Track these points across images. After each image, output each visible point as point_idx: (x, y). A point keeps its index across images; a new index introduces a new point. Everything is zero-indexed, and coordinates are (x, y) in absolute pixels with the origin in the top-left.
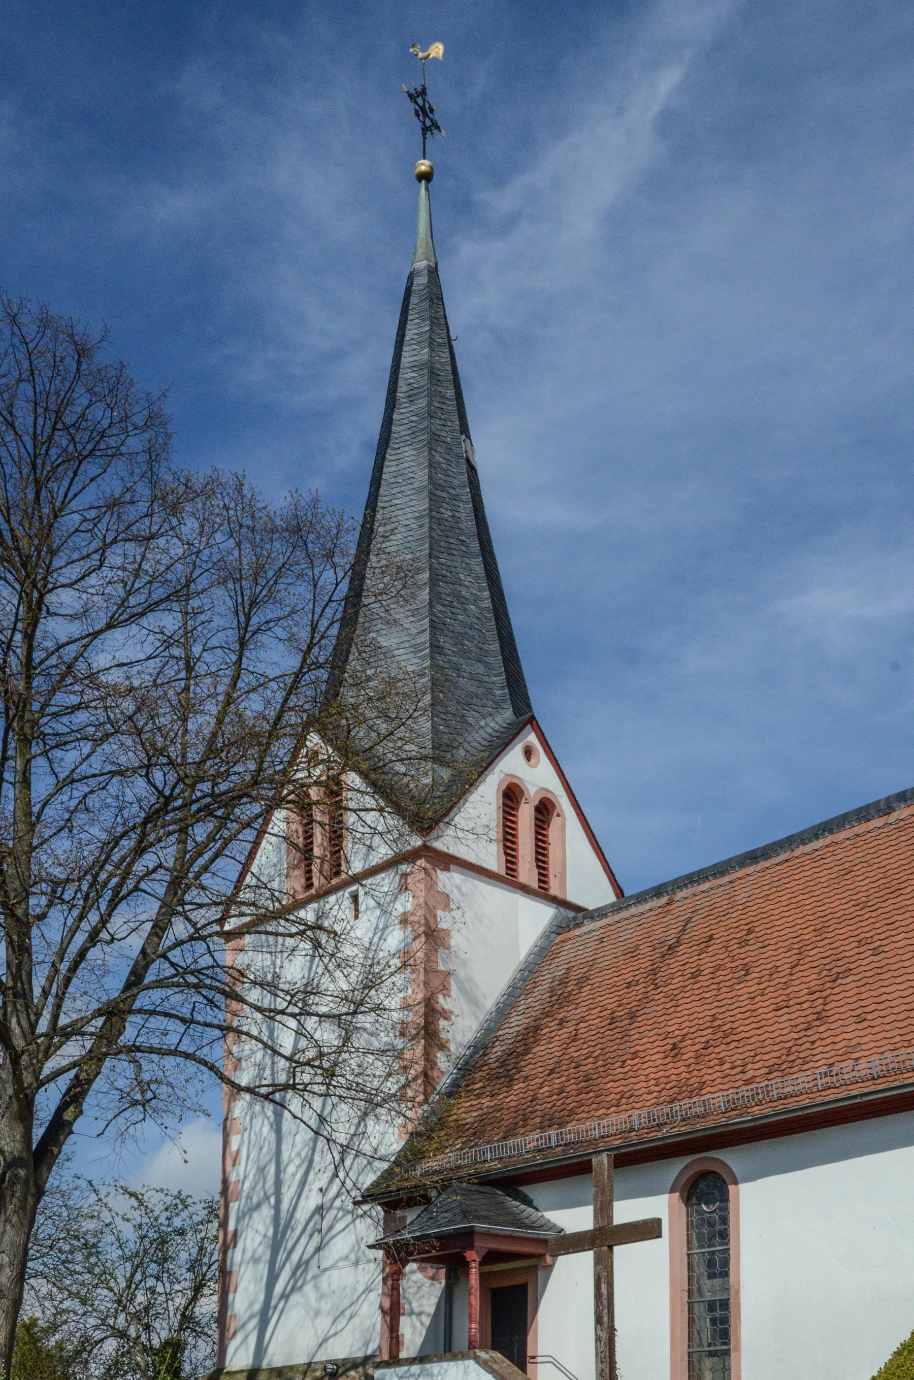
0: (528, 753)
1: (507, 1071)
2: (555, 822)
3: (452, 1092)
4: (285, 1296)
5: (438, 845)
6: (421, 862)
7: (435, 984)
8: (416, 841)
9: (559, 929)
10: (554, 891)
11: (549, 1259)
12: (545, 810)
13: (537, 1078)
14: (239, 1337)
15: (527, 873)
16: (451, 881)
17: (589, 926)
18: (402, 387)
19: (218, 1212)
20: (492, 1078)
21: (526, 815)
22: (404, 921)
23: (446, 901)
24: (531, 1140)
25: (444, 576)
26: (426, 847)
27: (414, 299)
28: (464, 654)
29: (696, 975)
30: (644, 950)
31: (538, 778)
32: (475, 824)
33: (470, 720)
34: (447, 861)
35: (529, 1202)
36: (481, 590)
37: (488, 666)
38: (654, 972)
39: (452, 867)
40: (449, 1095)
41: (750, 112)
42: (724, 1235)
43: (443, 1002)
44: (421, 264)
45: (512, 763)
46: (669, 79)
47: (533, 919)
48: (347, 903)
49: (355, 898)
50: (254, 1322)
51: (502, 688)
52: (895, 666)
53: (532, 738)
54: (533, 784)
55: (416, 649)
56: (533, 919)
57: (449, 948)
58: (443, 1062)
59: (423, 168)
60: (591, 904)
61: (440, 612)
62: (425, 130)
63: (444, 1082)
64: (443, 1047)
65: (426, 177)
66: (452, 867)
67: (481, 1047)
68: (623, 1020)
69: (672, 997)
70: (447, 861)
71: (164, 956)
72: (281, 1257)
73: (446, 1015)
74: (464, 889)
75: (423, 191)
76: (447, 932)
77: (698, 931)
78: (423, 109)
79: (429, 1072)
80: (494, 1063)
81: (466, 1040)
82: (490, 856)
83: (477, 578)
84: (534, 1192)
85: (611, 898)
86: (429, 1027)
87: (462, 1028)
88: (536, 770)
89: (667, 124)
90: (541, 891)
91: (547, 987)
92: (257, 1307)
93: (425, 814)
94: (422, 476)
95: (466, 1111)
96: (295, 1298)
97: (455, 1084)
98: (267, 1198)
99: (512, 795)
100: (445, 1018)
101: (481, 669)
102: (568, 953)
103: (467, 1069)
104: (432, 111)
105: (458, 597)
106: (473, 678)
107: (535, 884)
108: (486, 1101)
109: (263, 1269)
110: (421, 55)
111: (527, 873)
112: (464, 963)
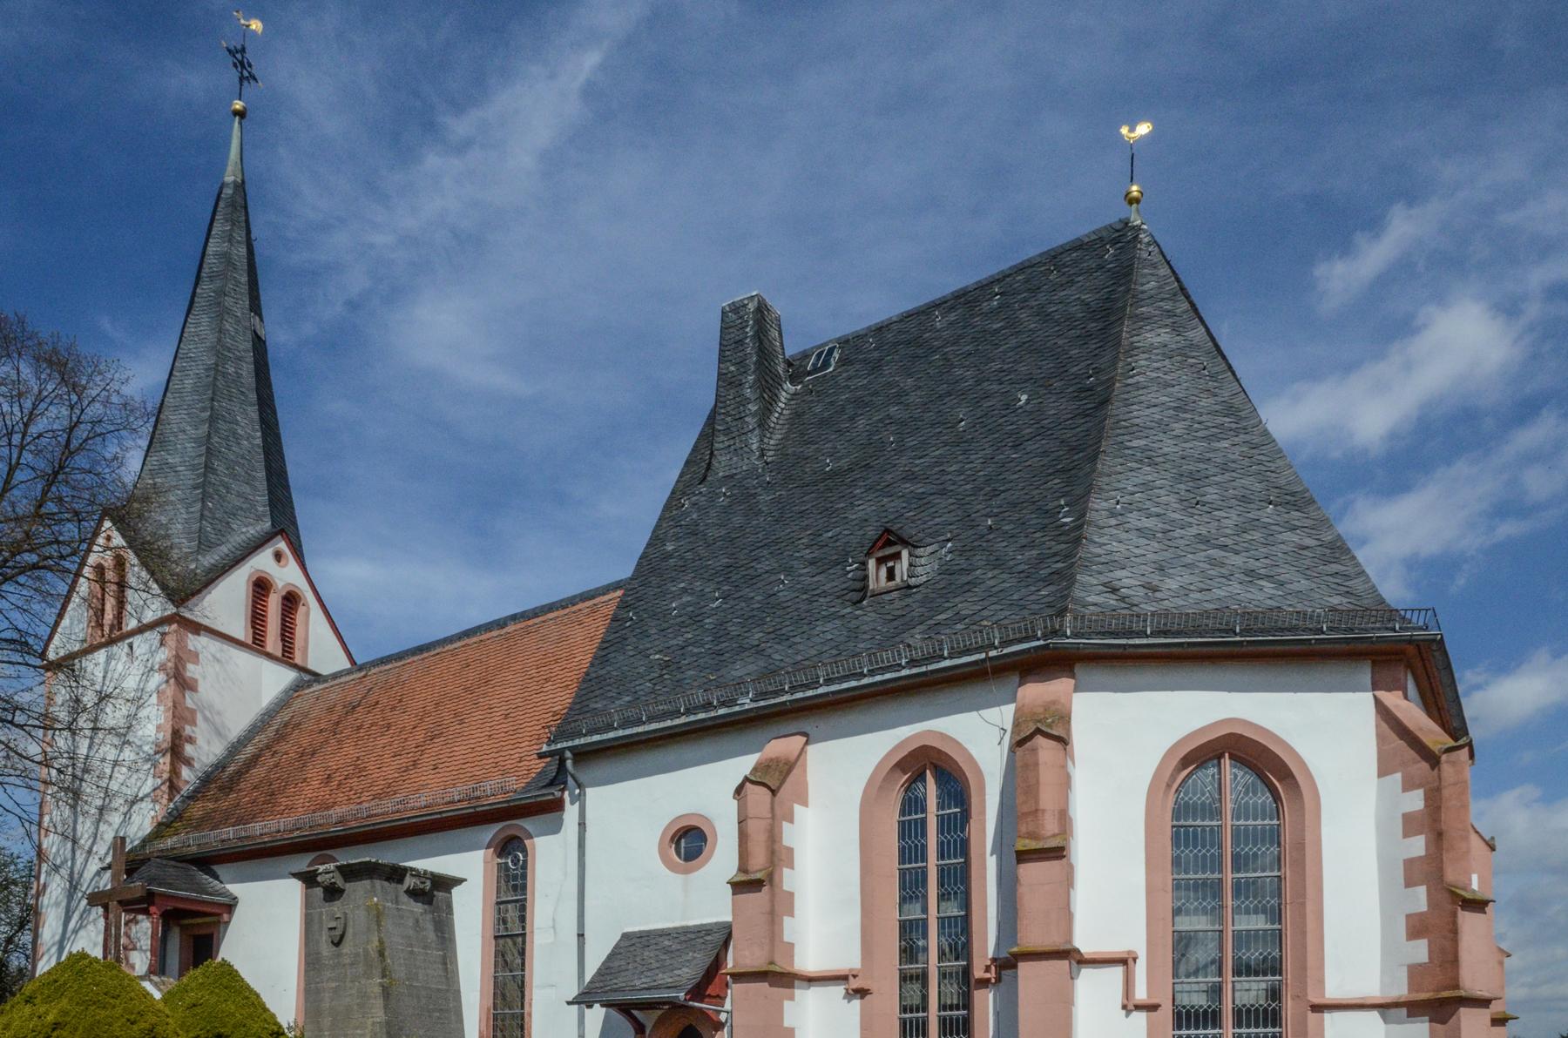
0: (278, 556)
1: (230, 785)
2: (301, 610)
3: (192, 797)
4: (76, 932)
5: (187, 615)
6: (174, 626)
8: (171, 609)
9: (297, 687)
10: (298, 660)
11: (225, 917)
12: (291, 601)
13: (244, 795)
14: (45, 958)
15: (273, 643)
17: (316, 687)
18: (206, 269)
19: (32, 873)
20: (221, 789)
21: (274, 604)
22: (162, 668)
24: (229, 832)
26: (177, 614)
27: (221, 204)
28: (234, 476)
29: (359, 728)
30: (339, 708)
31: (287, 575)
32: (225, 604)
35: (216, 877)
37: (254, 488)
38: (338, 723)
41: (653, 94)
43: (188, 730)
45: (263, 561)
46: (592, 59)
47: (273, 680)
48: (126, 649)
49: (131, 647)
50: (54, 949)
53: (282, 545)
55: (193, 468)
56: (273, 680)
58: (185, 773)
60: (325, 671)
62: (242, 79)
63: (186, 789)
64: (188, 762)
65: (241, 114)
67: (220, 766)
68: (307, 755)
69: (340, 742)
72: (74, 904)
73: (191, 740)
75: (236, 125)
77: (372, 699)
78: (242, 63)
80: (218, 780)
82: (240, 630)
83: (252, 421)
84: (219, 869)
86: (176, 748)
87: (206, 750)
88: (285, 570)
89: (590, 92)
90: (286, 657)
91: (275, 727)
92: (57, 938)
93: (183, 592)
94: (212, 338)
95: (197, 810)
96: (82, 933)
98: (66, 861)
99: (261, 586)
101: (248, 490)
102: (297, 705)
103: (207, 780)
105: (235, 433)
108: (211, 805)
109: (61, 911)
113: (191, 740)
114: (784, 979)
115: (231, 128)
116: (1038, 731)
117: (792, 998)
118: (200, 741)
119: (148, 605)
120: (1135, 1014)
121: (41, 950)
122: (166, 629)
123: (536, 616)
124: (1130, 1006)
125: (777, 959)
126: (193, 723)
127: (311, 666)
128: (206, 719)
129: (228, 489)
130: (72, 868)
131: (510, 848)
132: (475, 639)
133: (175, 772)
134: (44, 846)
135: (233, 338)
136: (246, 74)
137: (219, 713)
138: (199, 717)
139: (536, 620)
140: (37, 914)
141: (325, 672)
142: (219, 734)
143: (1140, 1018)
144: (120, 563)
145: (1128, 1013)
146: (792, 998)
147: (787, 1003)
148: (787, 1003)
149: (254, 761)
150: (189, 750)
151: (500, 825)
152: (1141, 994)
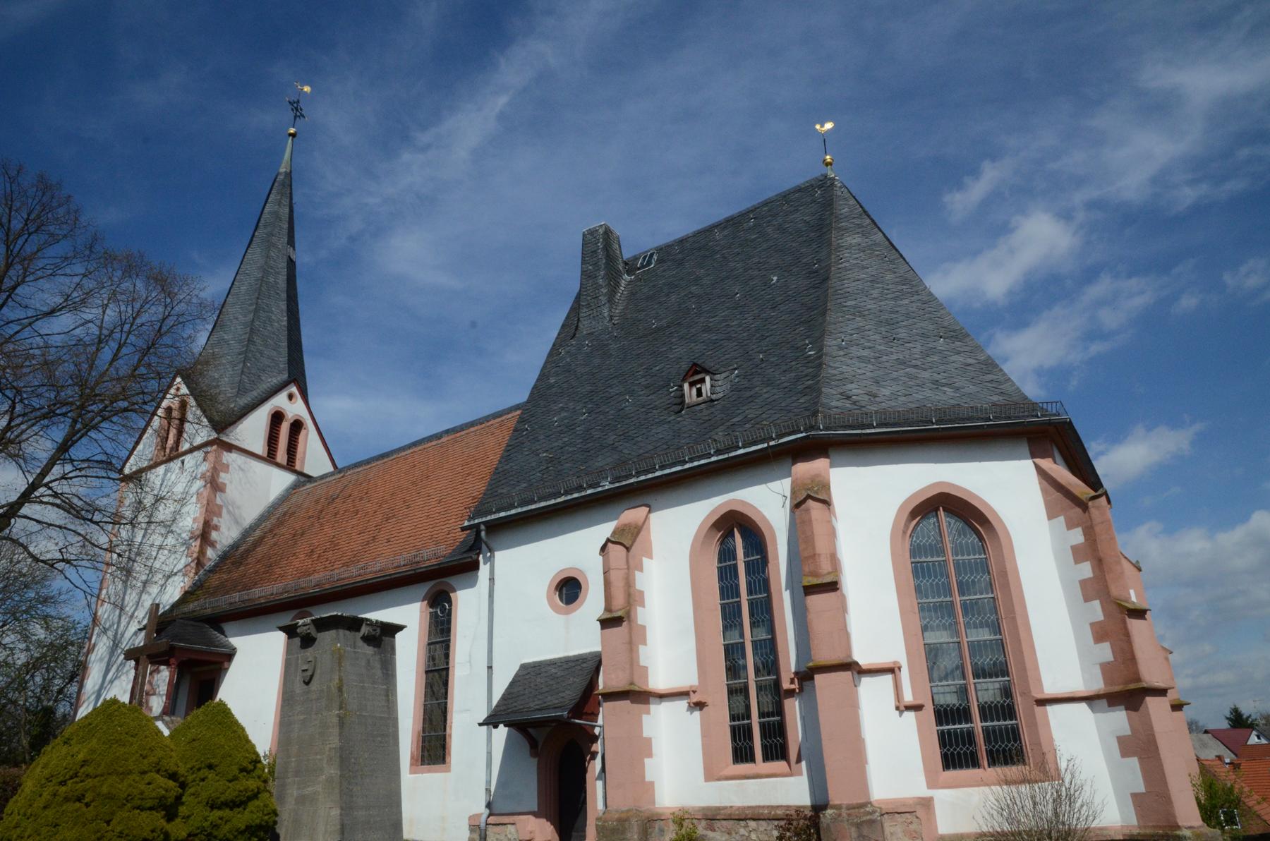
0: (291, 397)
2: (303, 432)
3: (212, 571)
4: (111, 682)
5: (225, 439)
7: (211, 513)
9: (295, 487)
10: (298, 467)
11: (226, 664)
12: (297, 426)
15: (282, 456)
16: (231, 458)
17: (309, 486)
19: (87, 634)
31: (294, 409)
32: (252, 431)
34: (230, 448)
35: (223, 633)
40: (210, 571)
42: (449, 630)
43: (215, 520)
44: (282, 170)
45: (280, 401)
48: (179, 464)
49: (183, 462)
53: (294, 389)
56: (280, 481)
58: (211, 553)
60: (314, 473)
63: (209, 565)
64: (213, 545)
65: (293, 135)
67: (235, 546)
70: (230, 448)
71: (46, 485)
72: (114, 659)
73: (216, 528)
80: (234, 556)
82: (260, 447)
85: (331, 469)
87: (226, 535)
90: (290, 466)
92: (97, 688)
93: (223, 422)
96: (116, 683)
97: (216, 566)
99: (277, 417)
102: (294, 499)
103: (224, 557)
105: (270, 318)
106: (269, 357)
107: (285, 463)
109: (104, 665)
111: (282, 456)
113: (216, 528)
114: (640, 696)
117: (648, 713)
118: (223, 529)
120: (907, 714)
124: (903, 708)
125: (636, 681)
126: (220, 515)
127: (306, 471)
128: (229, 512)
129: (262, 354)
133: (202, 552)
137: (239, 508)
138: (224, 511)
142: (237, 522)
143: (910, 716)
145: (901, 712)
146: (648, 713)
147: (645, 717)
148: (645, 717)
149: (260, 541)
150: (214, 535)
152: (908, 697)
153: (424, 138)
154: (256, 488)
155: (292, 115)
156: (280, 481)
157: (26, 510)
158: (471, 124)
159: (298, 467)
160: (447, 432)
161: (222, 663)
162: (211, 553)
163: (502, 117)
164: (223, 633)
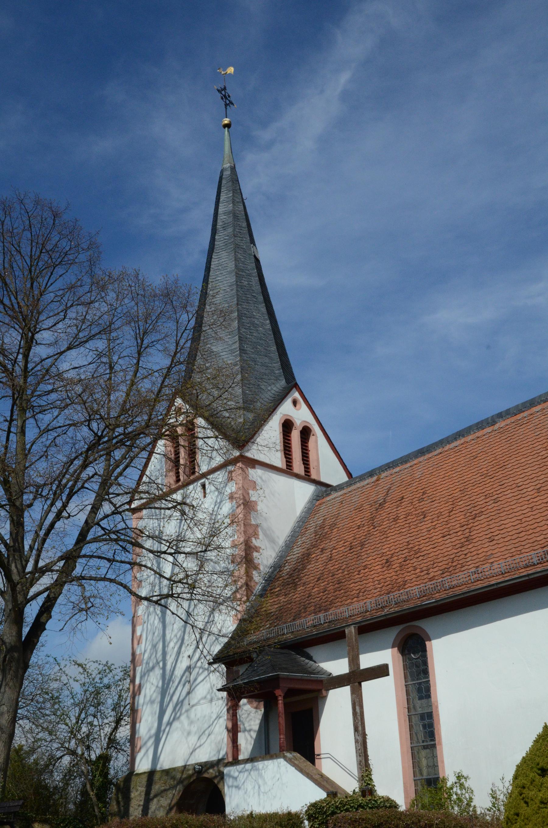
0: (295, 403)
2: (312, 439)
3: (263, 594)
4: (170, 724)
5: (249, 455)
6: (239, 464)
7: (250, 531)
8: (237, 453)
9: (317, 497)
12: (306, 432)
15: (298, 467)
17: (334, 495)
18: (220, 223)
19: (129, 673)
20: (285, 584)
21: (295, 436)
22: (231, 497)
23: (254, 485)
25: (245, 314)
27: (224, 182)
29: (396, 519)
31: (301, 416)
32: (268, 442)
33: (263, 387)
34: (254, 463)
36: (265, 320)
37: (271, 358)
38: (373, 519)
39: (257, 466)
40: (261, 596)
43: (255, 542)
45: (286, 409)
48: (199, 489)
49: (204, 486)
50: (152, 741)
51: (279, 369)
52: (488, 347)
53: (296, 395)
54: (298, 419)
55: (232, 352)
57: (257, 511)
59: (226, 122)
60: (334, 483)
61: (244, 332)
62: (226, 105)
63: (258, 588)
64: (256, 568)
65: (228, 126)
66: (257, 466)
67: (277, 567)
70: (254, 463)
72: (167, 699)
74: (264, 478)
75: (226, 132)
76: (255, 502)
78: (225, 96)
79: (249, 583)
80: (285, 576)
81: (269, 563)
82: (278, 460)
83: (263, 314)
85: (345, 479)
87: (266, 557)
90: (307, 477)
91: (312, 530)
92: (153, 731)
93: (240, 438)
96: (176, 724)
97: (264, 589)
98: (158, 663)
99: (287, 426)
100: (257, 551)
101: (267, 360)
102: (323, 510)
103: (271, 580)
104: (229, 96)
105: (253, 324)
106: (263, 365)
109: (156, 707)
110: (223, 73)
111: (298, 467)
112: (266, 519)
115: (224, 133)
116: (86, 619)
119: (212, 450)
121: (139, 744)
122: (230, 468)
123: (521, 411)
127: (323, 479)
129: (255, 361)
130: (164, 668)
131: (414, 650)
132: (470, 438)
134: (138, 652)
135: (243, 263)
136: (228, 102)
139: (525, 414)
140: (134, 711)
141: (334, 484)
144: (190, 427)
149: (306, 558)
151: (401, 627)
153: (265, 135)
154: (284, 502)
155: (223, 103)
156: (304, 492)
157: (87, 550)
158: (314, 110)
159: (314, 476)
160: (500, 416)
161: (320, 691)
162: (258, 578)
163: (345, 96)
164: (310, 658)
